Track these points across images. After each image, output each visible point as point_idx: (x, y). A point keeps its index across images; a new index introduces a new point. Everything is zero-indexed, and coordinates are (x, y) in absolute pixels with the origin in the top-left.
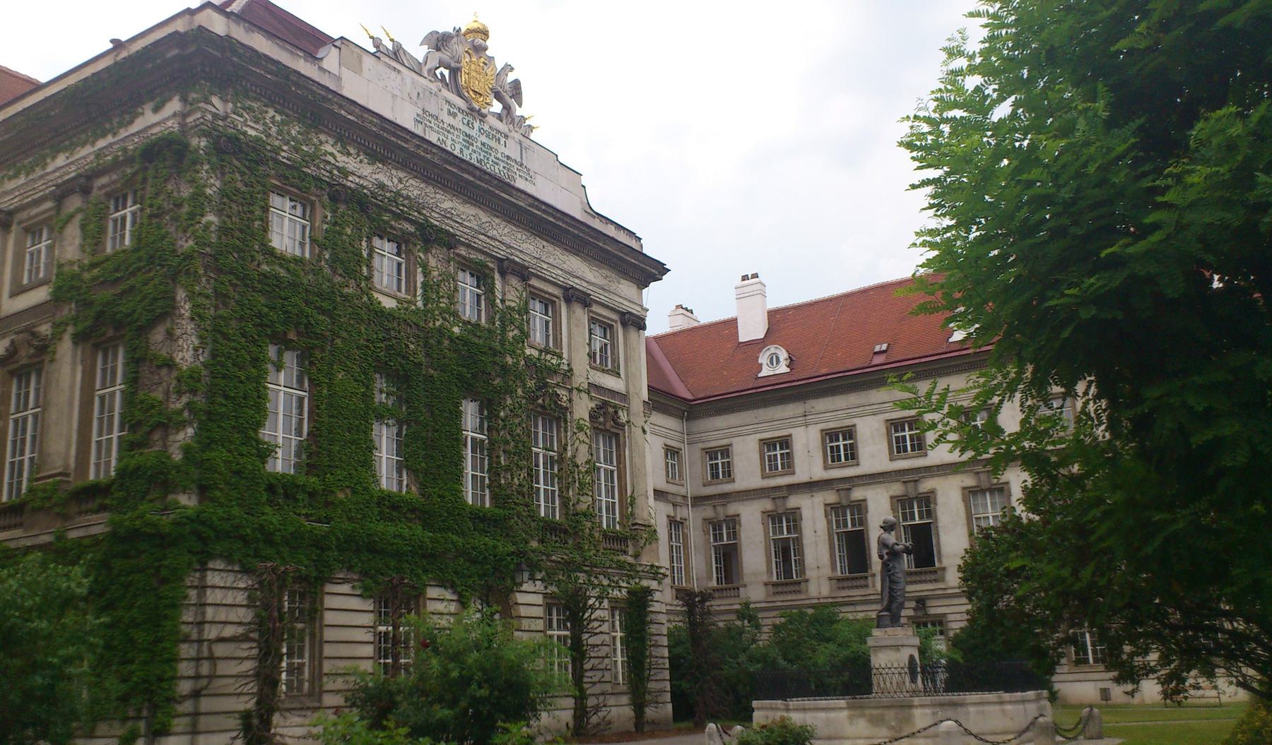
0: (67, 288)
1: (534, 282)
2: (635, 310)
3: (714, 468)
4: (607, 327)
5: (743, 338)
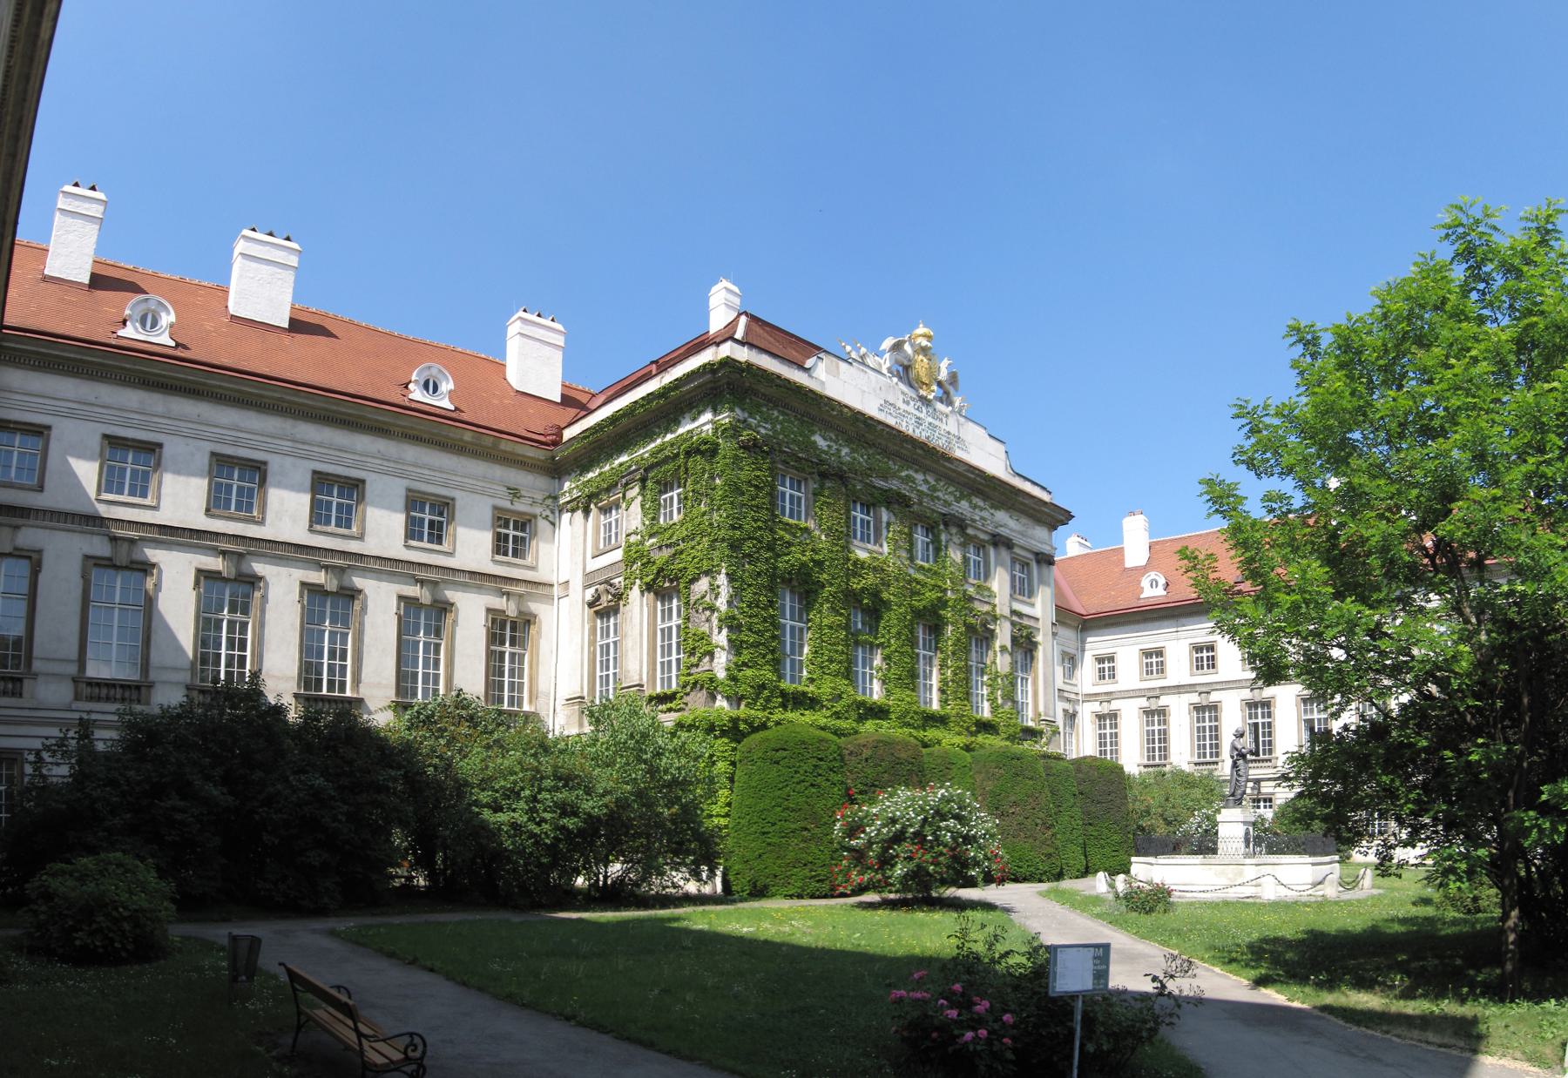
0: (635, 556)
1: (970, 531)
2: (1046, 549)
3: (1102, 670)
4: (1025, 565)
5: (1129, 563)
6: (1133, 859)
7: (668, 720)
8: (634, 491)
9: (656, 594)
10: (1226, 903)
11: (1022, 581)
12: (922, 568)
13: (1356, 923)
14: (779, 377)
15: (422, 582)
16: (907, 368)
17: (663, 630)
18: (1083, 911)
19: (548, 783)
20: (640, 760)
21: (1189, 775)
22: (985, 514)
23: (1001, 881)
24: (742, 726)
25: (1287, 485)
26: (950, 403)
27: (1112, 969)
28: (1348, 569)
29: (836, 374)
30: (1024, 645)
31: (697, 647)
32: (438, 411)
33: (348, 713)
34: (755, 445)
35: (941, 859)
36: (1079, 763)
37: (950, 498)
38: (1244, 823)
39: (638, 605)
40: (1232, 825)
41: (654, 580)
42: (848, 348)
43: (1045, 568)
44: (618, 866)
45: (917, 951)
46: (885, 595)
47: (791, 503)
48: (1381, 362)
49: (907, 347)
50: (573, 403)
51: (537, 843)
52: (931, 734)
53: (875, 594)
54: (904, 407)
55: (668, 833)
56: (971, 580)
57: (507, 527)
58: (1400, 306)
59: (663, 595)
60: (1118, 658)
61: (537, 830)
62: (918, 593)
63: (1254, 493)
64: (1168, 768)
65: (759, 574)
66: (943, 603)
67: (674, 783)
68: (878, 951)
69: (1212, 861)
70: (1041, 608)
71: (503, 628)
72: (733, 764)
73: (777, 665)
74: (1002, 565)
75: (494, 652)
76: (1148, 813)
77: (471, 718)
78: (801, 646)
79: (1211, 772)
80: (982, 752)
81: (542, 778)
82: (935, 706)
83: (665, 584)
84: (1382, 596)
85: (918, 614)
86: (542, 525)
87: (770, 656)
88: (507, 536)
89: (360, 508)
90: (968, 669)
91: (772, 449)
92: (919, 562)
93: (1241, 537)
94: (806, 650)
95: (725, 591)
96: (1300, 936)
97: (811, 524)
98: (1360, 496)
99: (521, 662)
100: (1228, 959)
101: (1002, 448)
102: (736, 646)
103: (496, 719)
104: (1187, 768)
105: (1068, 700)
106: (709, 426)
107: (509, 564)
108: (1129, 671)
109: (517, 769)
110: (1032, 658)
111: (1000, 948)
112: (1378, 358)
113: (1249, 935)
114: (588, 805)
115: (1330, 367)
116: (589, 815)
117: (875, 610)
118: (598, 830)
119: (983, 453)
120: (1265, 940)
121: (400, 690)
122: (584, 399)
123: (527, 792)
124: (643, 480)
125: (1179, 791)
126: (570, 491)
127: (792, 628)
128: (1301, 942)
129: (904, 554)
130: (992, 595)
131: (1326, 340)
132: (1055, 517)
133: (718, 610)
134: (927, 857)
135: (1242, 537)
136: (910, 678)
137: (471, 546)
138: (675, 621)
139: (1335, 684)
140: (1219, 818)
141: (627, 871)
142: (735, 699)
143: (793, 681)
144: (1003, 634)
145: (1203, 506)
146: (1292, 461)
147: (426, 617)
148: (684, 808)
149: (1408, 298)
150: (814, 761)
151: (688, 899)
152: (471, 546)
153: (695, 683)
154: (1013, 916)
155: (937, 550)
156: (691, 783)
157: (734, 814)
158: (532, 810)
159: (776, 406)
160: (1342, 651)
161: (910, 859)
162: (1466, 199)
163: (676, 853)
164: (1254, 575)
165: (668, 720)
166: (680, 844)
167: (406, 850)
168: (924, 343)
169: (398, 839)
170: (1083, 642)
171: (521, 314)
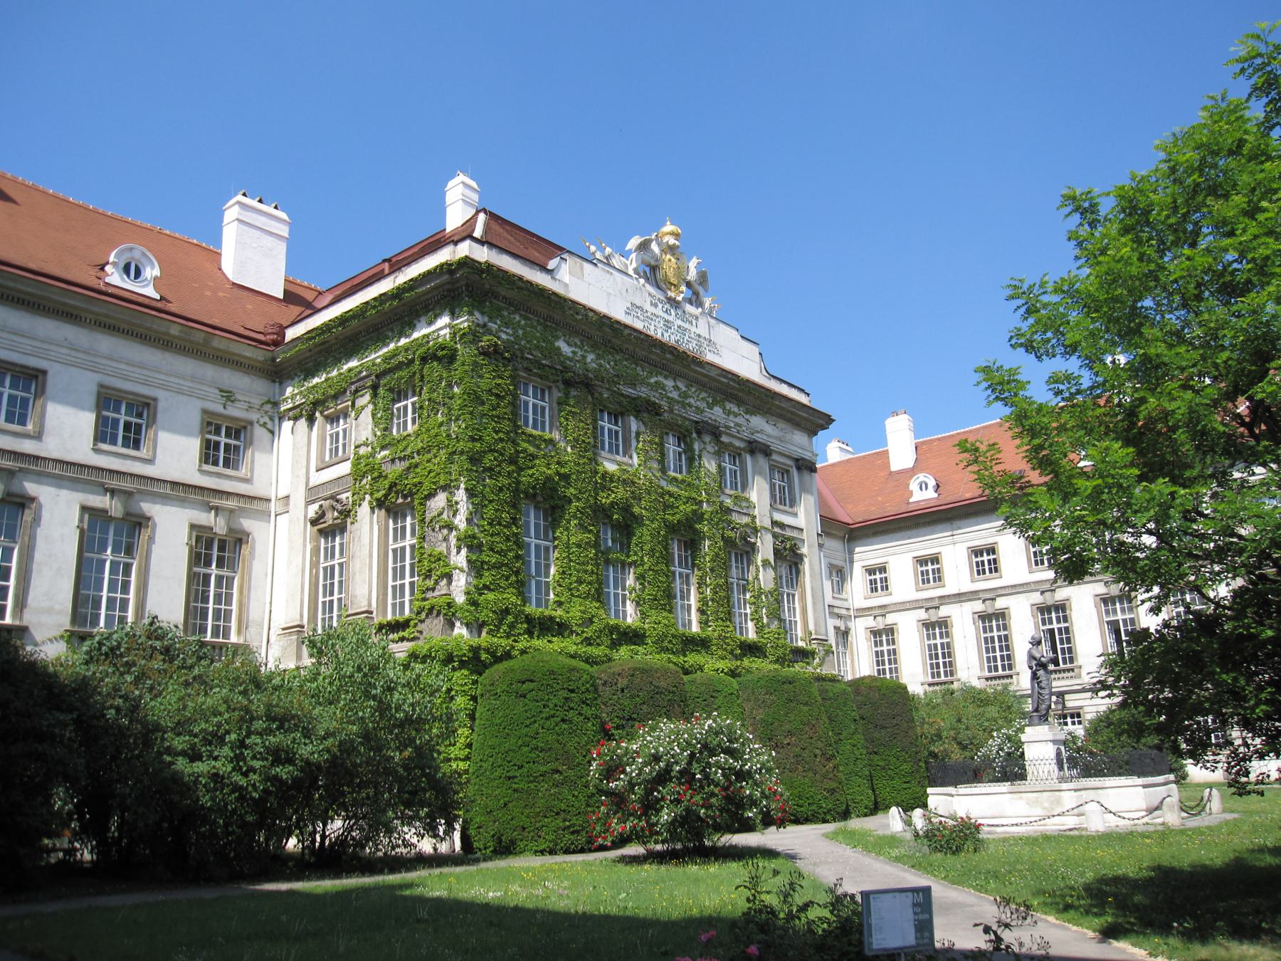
0: (364, 469)
1: (724, 439)
2: (807, 455)
4: (785, 472)
5: (895, 467)
6: (929, 790)
7: (400, 650)
8: (365, 399)
9: (388, 511)
10: (1047, 838)
11: (782, 489)
12: (675, 479)
13: (1215, 856)
14: (520, 278)
15: (113, 492)
16: (654, 269)
17: (395, 551)
18: (878, 854)
19: (259, 725)
20: (367, 696)
21: (980, 692)
22: (739, 420)
23: (781, 823)
24: (484, 656)
25: (1073, 365)
26: (699, 304)
27: (937, 921)
28: (1152, 448)
29: (581, 276)
30: (789, 557)
31: (432, 569)
32: (140, 299)
33: (8, 642)
34: (496, 351)
35: (713, 800)
36: (858, 684)
37: (703, 405)
38: (1054, 742)
39: (367, 525)
40: (1039, 745)
41: (386, 496)
42: (593, 248)
43: (806, 475)
44: (338, 823)
45: (695, 912)
46: (636, 510)
47: (535, 413)
48: (1172, 220)
49: (655, 247)
50: (298, 300)
51: (242, 798)
52: (692, 659)
53: (626, 509)
54: (651, 309)
55: (400, 780)
56: (728, 491)
57: (218, 432)
58: (1191, 156)
59: (395, 512)
60: (890, 568)
61: (243, 782)
62: (672, 507)
63: (1038, 379)
64: (956, 686)
65: (501, 489)
66: (699, 516)
67: (408, 720)
68: (650, 914)
69: (1022, 788)
70: (804, 518)
71: (209, 545)
72: (474, 698)
73: (521, 587)
74: (760, 474)
75: (197, 575)
76: (939, 737)
77: (166, 650)
78: (548, 567)
79: (1006, 687)
80: (749, 677)
81: (252, 719)
82: (695, 628)
83: (397, 501)
84: (1195, 472)
85: (672, 529)
86: (259, 432)
87: (513, 578)
88: (217, 444)
89: (39, 403)
90: (728, 587)
91: (514, 355)
92: (672, 474)
93: (1027, 423)
94: (553, 571)
95: (464, 508)
96: (1145, 874)
97: (556, 436)
98: (1157, 367)
99: (230, 585)
100: (1064, 907)
101: (756, 350)
102: (476, 568)
103: (194, 652)
104: (978, 684)
105: (840, 617)
106: (447, 331)
107: (219, 475)
108: (903, 582)
109: (223, 708)
110: (798, 572)
111: (799, 899)
112: (1168, 217)
113: (1082, 874)
114: (307, 751)
115: (1114, 232)
116: (308, 763)
117: (626, 526)
118: (317, 780)
119: (736, 356)
120: (1103, 880)
121: (76, 616)
122: (309, 296)
123: (233, 736)
124: (375, 388)
125: (972, 710)
126: (293, 397)
127: (537, 546)
128: (1150, 880)
129: (655, 465)
130: (751, 506)
131: (1107, 206)
132: (815, 422)
133: (456, 528)
134: (697, 798)
135: (1027, 422)
136: (666, 599)
137: (175, 453)
138: (409, 541)
139: (1152, 575)
140: (1023, 738)
141: (350, 829)
142: (476, 626)
143: (538, 605)
144: (765, 548)
145: (982, 393)
146: (1078, 337)
147: (115, 531)
148: (418, 749)
149: (1198, 147)
150: (565, 694)
151: (422, 861)
152: (175, 453)
153: (431, 609)
154: (799, 864)
155: (691, 460)
156: (426, 721)
157: (475, 757)
158: (239, 758)
159: (517, 310)
160: (1154, 539)
161: (677, 801)
162: (1264, 25)
163: (408, 805)
164: (1045, 464)
165: (400, 650)
166: (414, 793)
167: (70, 814)
168: (672, 241)
169: (61, 800)
170: (851, 553)
171: (240, 198)
